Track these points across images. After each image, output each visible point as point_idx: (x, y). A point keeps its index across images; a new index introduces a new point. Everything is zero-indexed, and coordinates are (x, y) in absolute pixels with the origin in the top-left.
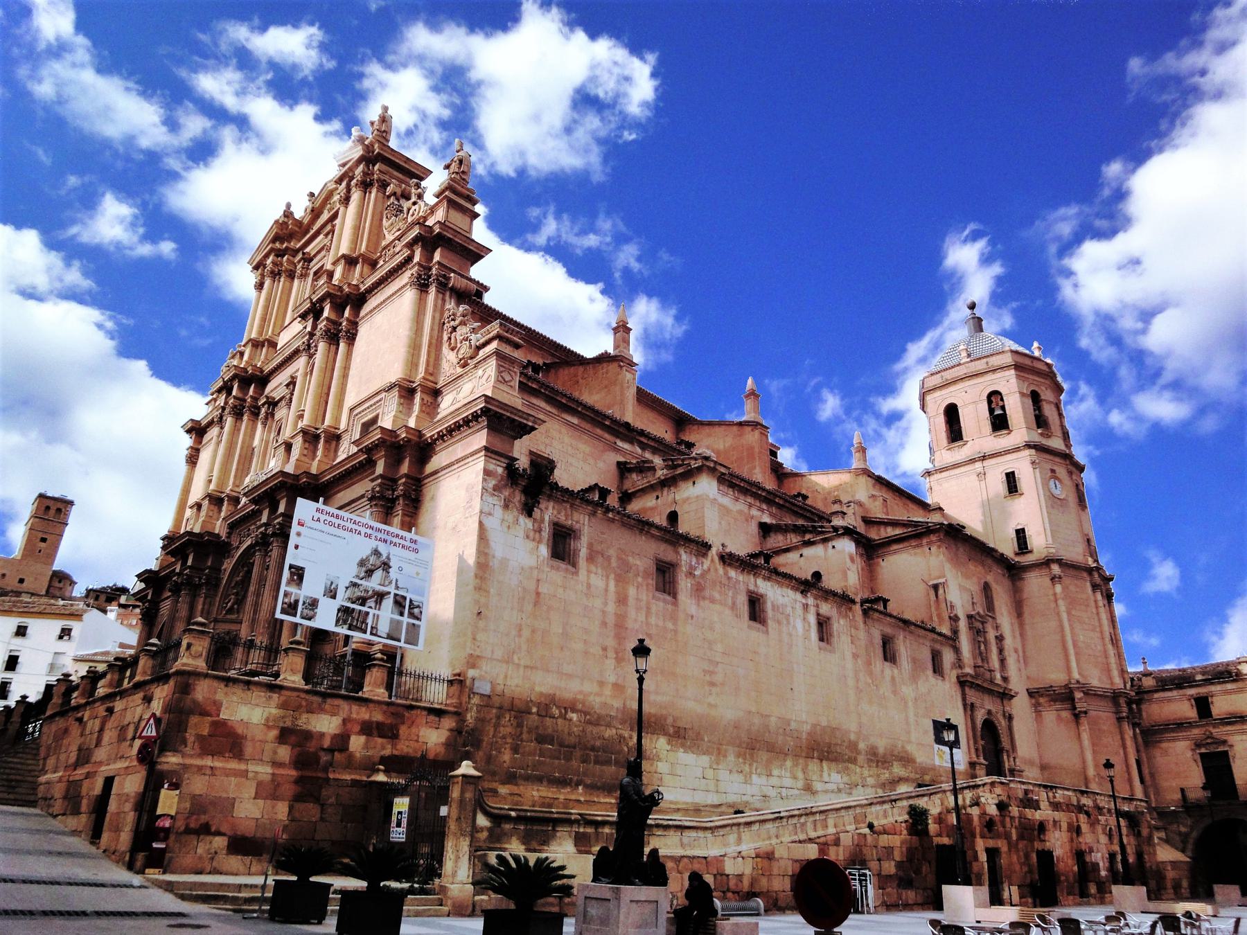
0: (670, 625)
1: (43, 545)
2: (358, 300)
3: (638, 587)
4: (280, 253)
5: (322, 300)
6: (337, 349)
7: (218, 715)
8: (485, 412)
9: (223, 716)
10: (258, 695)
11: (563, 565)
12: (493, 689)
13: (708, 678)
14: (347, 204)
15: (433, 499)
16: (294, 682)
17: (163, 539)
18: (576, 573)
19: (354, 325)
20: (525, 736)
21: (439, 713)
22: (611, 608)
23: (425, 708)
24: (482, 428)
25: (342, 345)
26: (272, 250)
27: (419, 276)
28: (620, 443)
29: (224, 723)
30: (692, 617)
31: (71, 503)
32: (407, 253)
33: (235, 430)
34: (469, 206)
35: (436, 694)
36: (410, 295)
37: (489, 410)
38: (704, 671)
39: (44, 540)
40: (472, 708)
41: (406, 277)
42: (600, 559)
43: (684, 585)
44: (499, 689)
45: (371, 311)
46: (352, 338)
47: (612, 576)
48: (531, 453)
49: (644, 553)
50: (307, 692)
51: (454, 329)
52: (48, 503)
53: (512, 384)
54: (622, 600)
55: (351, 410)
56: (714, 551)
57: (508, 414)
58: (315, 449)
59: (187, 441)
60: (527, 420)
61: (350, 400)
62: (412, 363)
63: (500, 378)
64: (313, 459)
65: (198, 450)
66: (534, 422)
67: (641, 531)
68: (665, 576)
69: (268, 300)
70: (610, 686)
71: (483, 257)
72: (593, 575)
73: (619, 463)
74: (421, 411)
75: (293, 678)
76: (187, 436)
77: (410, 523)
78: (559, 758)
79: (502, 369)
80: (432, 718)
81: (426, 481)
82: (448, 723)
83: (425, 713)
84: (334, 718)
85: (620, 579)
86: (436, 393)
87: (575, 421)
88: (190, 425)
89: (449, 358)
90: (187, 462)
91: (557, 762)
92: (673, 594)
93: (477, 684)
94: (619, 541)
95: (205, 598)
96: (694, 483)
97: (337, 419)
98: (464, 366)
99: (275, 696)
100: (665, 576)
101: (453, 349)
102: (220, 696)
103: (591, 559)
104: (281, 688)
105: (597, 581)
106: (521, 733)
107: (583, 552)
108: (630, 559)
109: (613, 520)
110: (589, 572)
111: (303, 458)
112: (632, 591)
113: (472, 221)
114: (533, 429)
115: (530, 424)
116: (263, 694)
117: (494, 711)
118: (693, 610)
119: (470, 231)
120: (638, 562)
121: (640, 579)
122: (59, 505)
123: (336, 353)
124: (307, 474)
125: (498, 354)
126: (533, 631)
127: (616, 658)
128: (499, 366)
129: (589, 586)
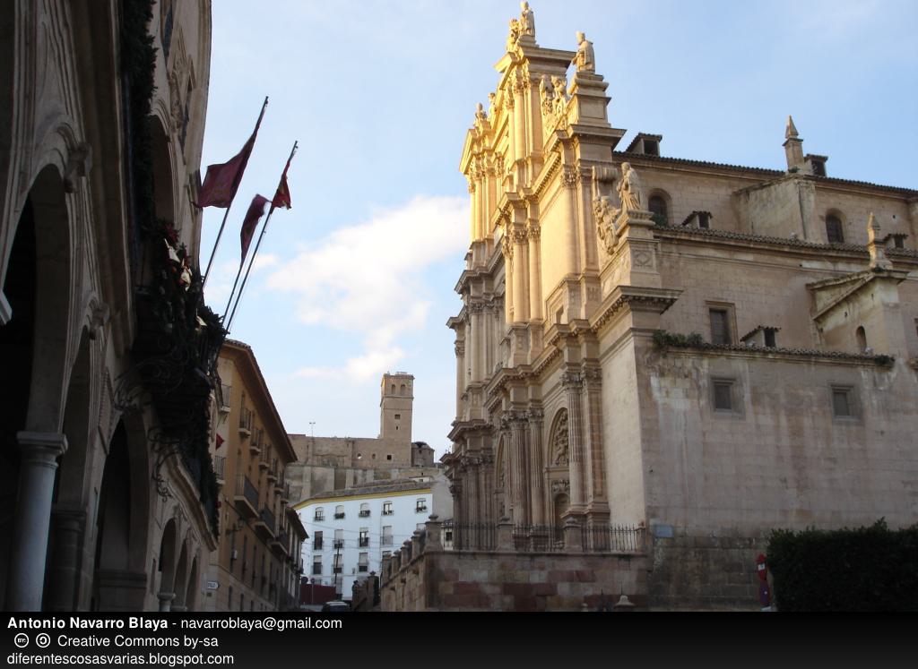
0: (856, 446)
1: (398, 421)
2: (534, 200)
3: (813, 417)
4: (478, 156)
5: (506, 208)
6: (528, 248)
7: (457, 579)
8: (624, 298)
9: (461, 579)
10: (483, 562)
11: (726, 413)
12: (674, 533)
13: (909, 488)
14: (513, 108)
15: (609, 376)
16: (507, 549)
17: (453, 425)
18: (743, 418)
19: (535, 222)
20: (712, 567)
21: (626, 557)
22: (786, 442)
23: (615, 555)
24: (627, 313)
25: (531, 244)
26: (472, 155)
27: (567, 176)
28: (806, 264)
29: (464, 584)
30: (882, 433)
31: (412, 378)
32: (555, 155)
33: (479, 325)
34: (598, 93)
35: (631, 543)
36: (564, 196)
37: (627, 296)
38: (903, 482)
39: (397, 416)
40: (658, 550)
41: (557, 182)
42: (766, 400)
43: (870, 400)
44: (679, 531)
45: (546, 209)
46: (537, 236)
47: (783, 412)
48: (708, 302)
49: (814, 382)
50: (518, 555)
51: (601, 220)
52: (392, 381)
53: (649, 263)
54: (796, 432)
55: (547, 301)
56: (900, 361)
57: (646, 295)
58: (528, 340)
59: (453, 335)
60: (665, 294)
61: (545, 294)
62: (575, 258)
63: (637, 262)
64: (528, 350)
65: (463, 342)
66: (673, 294)
67: (809, 362)
68: (843, 401)
69: (481, 197)
70: (794, 513)
71: (620, 138)
72: (760, 416)
73: (807, 285)
74: (589, 299)
75: (505, 547)
76: (453, 330)
77: (321, 548)
78: (750, 582)
79: (636, 253)
80: (623, 562)
81: (603, 360)
82: (637, 565)
83: (616, 559)
84: (542, 573)
85: (791, 413)
86: (597, 280)
87: (750, 257)
88: (451, 322)
89: (601, 246)
90: (457, 354)
91: (748, 585)
92: (860, 415)
93: (659, 530)
94: (783, 376)
95: (486, 474)
96: (872, 295)
97: (539, 310)
98: (612, 253)
99: (495, 561)
100: (843, 401)
101: (603, 239)
102: (456, 566)
103: (756, 400)
104: (498, 554)
105: (766, 420)
106: (708, 565)
107: (747, 396)
108: (801, 392)
109: (774, 360)
110: (756, 413)
111: (520, 352)
112: (807, 422)
113: (605, 107)
114: (673, 301)
115: (669, 297)
116: (485, 561)
117: (679, 550)
118: (883, 425)
119: (605, 117)
120: (811, 394)
121: (815, 409)
122: (402, 382)
123: (528, 251)
124: (578, 321)
125: (630, 241)
126: (706, 479)
127: (798, 487)
128: (633, 252)
129: (758, 427)
